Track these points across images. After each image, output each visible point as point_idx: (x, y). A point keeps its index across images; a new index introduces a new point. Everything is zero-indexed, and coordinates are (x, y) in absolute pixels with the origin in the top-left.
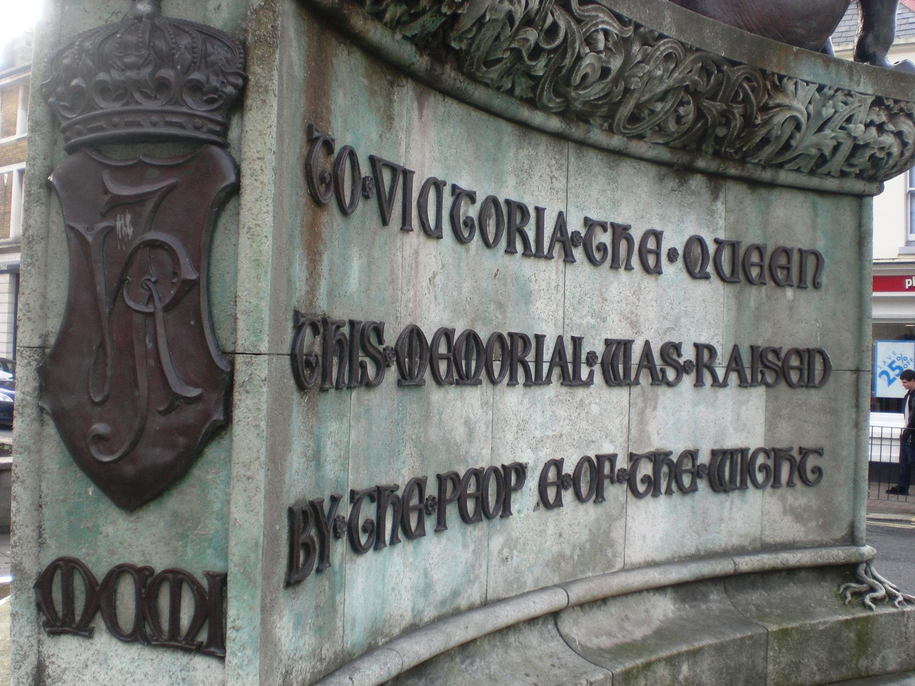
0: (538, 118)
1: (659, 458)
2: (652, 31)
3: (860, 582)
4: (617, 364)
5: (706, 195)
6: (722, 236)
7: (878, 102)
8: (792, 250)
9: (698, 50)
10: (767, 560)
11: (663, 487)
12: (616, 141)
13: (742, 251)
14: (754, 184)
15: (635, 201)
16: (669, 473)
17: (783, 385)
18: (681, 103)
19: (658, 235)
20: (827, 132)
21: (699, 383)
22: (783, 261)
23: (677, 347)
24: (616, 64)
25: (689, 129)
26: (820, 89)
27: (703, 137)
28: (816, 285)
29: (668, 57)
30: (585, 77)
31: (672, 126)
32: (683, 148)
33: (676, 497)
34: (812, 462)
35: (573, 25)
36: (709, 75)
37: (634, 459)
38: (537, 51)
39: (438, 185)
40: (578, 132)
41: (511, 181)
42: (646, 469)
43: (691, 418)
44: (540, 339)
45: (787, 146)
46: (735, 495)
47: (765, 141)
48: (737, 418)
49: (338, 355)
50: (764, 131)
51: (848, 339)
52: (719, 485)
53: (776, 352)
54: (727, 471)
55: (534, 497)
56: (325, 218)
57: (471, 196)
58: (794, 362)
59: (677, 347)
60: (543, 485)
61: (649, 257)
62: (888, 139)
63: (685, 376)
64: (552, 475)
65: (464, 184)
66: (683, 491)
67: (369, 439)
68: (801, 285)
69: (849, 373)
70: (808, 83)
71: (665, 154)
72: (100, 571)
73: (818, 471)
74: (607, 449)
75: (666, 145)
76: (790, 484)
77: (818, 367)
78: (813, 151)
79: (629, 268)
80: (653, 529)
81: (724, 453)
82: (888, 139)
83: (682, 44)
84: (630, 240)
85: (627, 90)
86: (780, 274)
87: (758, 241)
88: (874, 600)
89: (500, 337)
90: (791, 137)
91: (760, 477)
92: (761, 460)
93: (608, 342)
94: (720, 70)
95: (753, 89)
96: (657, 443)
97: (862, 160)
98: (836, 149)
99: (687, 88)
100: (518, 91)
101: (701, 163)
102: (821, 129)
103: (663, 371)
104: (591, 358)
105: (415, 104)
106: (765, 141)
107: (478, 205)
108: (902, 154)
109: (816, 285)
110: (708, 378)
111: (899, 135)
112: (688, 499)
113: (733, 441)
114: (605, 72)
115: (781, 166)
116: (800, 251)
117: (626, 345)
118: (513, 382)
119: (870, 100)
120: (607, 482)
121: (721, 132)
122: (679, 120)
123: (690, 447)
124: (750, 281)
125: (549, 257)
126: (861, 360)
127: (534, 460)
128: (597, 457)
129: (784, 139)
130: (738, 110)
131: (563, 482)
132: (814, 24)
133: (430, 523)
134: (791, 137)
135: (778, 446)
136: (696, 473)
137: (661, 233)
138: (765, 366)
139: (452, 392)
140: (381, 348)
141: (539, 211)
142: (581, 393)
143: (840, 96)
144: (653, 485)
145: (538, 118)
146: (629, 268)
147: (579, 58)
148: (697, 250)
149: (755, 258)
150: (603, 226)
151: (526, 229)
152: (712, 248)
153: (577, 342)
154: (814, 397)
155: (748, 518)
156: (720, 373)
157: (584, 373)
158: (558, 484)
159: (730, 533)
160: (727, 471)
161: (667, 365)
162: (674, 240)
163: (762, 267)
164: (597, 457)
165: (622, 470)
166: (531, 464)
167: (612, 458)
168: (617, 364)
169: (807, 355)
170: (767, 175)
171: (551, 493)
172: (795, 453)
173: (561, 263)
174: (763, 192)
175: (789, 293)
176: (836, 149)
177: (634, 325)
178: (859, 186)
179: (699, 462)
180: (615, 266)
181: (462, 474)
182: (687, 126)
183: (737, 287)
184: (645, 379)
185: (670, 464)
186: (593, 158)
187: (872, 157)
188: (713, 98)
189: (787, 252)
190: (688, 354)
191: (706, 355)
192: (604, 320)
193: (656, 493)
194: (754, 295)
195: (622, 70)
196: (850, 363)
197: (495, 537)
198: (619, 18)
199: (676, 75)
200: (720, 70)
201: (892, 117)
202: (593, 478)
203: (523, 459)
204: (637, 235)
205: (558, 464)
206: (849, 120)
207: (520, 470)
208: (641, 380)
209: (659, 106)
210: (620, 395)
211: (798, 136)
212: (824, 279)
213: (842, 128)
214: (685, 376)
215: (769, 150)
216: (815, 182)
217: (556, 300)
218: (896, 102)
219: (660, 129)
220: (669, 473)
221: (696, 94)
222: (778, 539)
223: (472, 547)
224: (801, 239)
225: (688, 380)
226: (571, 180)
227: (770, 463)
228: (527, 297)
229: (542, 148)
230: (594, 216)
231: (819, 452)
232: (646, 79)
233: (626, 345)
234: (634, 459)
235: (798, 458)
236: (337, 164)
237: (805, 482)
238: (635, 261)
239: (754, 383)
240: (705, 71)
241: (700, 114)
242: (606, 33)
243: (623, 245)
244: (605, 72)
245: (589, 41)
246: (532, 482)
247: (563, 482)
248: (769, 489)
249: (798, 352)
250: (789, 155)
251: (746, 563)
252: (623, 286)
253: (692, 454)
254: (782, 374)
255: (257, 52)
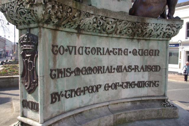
0: (102, 35)
1: (127, 83)
2: (121, 20)
3: (165, 102)
4: (119, 69)
5: (137, 42)
6: (140, 48)
7: (169, 25)
8: (153, 50)
9: (131, 21)
10: (148, 98)
11: (128, 87)
12: (118, 36)
13: (144, 51)
14: (146, 40)
15: (124, 44)
16: (130, 85)
17: (151, 71)
18: (129, 29)
19: (127, 50)
20: (158, 31)
21: (135, 71)
22: (152, 52)
23: (131, 66)
24: (114, 26)
25: (131, 33)
26: (156, 24)
27: (134, 34)
28: (158, 55)
29: (125, 23)
30: (108, 28)
31: (128, 33)
32: (131, 36)
33: (131, 88)
34: (157, 83)
35: (104, 22)
36: (133, 25)
37: (123, 83)
38: (98, 26)
39: (82, 47)
40: (111, 36)
41: (98, 44)
42: (125, 84)
43: (132, 77)
44: (104, 67)
45: (151, 34)
46: (142, 88)
47: (146, 33)
48: (144, 76)
49: (57, 73)
50: (146, 32)
51: (164, 64)
52: (139, 87)
53: (150, 66)
54: (141, 84)
55: (104, 89)
56: (57, 56)
57: (89, 48)
58: (154, 67)
59: (131, 66)
60: (105, 87)
61: (126, 52)
62: (171, 31)
63: (133, 70)
64: (107, 86)
65: (88, 46)
66: (132, 88)
67: (63, 84)
68: (155, 55)
69: (164, 69)
70: (154, 24)
71: (128, 37)
72: (88, 87)
73: (158, 84)
74: (118, 82)
75: (128, 36)
76: (153, 86)
77: (158, 68)
78: (156, 34)
79: (121, 55)
80: (126, 93)
81: (140, 82)
82: (171, 31)
83: (128, 21)
84: (122, 51)
85: (117, 29)
86: (151, 54)
87: (147, 49)
88: (167, 106)
89: (95, 67)
90: (151, 32)
91: (147, 85)
92: (147, 83)
93: (118, 66)
94: (135, 24)
95: (142, 26)
96: (127, 81)
97: (166, 35)
98: (161, 33)
99: (129, 27)
100: (97, 32)
101: (135, 38)
102: (157, 31)
103: (128, 70)
104: (114, 69)
105: (77, 37)
106: (146, 33)
107: (91, 49)
108: (174, 33)
109: (158, 55)
110: (137, 70)
111: (173, 30)
112: (133, 89)
113: (142, 80)
114: (112, 27)
115: (151, 37)
116: (155, 50)
117: (121, 66)
118: (99, 73)
119: (166, 25)
120: (117, 86)
121: (138, 33)
122: (129, 32)
123: (134, 81)
124: (145, 55)
125: (106, 54)
126: (166, 67)
127: (103, 84)
128: (116, 83)
129: (150, 33)
130: (140, 30)
131: (109, 87)
132: (156, 14)
133: (82, 94)
134: (151, 32)
135: (150, 81)
136: (135, 85)
137: (128, 49)
138: (148, 68)
139: (86, 76)
140: (71, 71)
141: (103, 48)
142: (112, 74)
143: (160, 25)
144: (126, 87)
145: (102, 35)
146: (121, 55)
147: (106, 26)
148: (135, 51)
149: (146, 51)
150: (116, 49)
151: (101, 51)
152: (138, 51)
153: (111, 67)
154: (157, 73)
155: (144, 91)
156: (139, 70)
157: (113, 71)
158: (107, 87)
159: (141, 94)
160: (141, 84)
161: (129, 69)
162: (130, 49)
163: (147, 53)
164: (116, 83)
165: (120, 85)
166: (102, 84)
167: (119, 83)
168: (119, 69)
169: (156, 67)
170: (148, 38)
171: (107, 88)
172: (154, 82)
173: (108, 55)
174: (148, 41)
175: (153, 57)
176: (161, 33)
177: (122, 63)
178: (166, 39)
179: (135, 83)
180: (119, 54)
181: (88, 87)
182: (131, 33)
183: (143, 56)
184: (125, 71)
185: (130, 83)
186: (114, 39)
187: (168, 34)
188: (135, 28)
189: (153, 50)
190: (133, 67)
191: (137, 67)
192: (117, 63)
193: (127, 88)
194: (146, 57)
195: (116, 26)
196: (164, 67)
197: (95, 95)
198: (114, 19)
199: (126, 26)
200: (135, 24)
201: (171, 27)
202: (115, 86)
203: (100, 84)
204: (123, 50)
205: (108, 84)
206: (163, 29)
207: (100, 86)
208: (124, 71)
209: (124, 31)
210: (120, 74)
211: (152, 32)
212: (159, 54)
213: (161, 30)
214: (133, 70)
215: (147, 35)
216: (158, 39)
217: (106, 61)
218: (172, 25)
219: (126, 33)
220: (130, 85)
221: (131, 28)
222: (150, 95)
223: (91, 96)
224: (155, 48)
225: (133, 71)
226: (110, 43)
227: (149, 83)
228: (101, 61)
229: (104, 39)
230: (114, 48)
231: (158, 82)
232: (121, 27)
233: (121, 66)
234: (123, 83)
235: (154, 82)
236: (60, 48)
237: (155, 86)
238: (123, 53)
239: (146, 71)
240: (133, 24)
241: (133, 31)
242: (111, 22)
243: (120, 51)
244: (112, 27)
245: (108, 23)
246: (103, 87)
247: (109, 87)
248: (149, 87)
249: (154, 66)
250: (151, 35)
251: (143, 99)
252: (119, 58)
253: (134, 82)
254: (151, 69)
255: (39, 38)
